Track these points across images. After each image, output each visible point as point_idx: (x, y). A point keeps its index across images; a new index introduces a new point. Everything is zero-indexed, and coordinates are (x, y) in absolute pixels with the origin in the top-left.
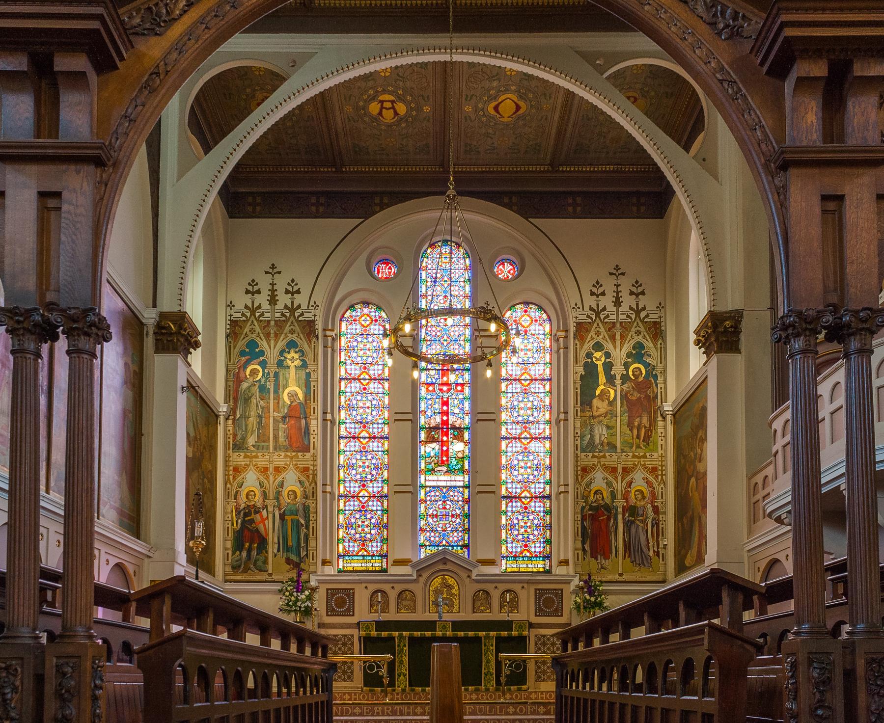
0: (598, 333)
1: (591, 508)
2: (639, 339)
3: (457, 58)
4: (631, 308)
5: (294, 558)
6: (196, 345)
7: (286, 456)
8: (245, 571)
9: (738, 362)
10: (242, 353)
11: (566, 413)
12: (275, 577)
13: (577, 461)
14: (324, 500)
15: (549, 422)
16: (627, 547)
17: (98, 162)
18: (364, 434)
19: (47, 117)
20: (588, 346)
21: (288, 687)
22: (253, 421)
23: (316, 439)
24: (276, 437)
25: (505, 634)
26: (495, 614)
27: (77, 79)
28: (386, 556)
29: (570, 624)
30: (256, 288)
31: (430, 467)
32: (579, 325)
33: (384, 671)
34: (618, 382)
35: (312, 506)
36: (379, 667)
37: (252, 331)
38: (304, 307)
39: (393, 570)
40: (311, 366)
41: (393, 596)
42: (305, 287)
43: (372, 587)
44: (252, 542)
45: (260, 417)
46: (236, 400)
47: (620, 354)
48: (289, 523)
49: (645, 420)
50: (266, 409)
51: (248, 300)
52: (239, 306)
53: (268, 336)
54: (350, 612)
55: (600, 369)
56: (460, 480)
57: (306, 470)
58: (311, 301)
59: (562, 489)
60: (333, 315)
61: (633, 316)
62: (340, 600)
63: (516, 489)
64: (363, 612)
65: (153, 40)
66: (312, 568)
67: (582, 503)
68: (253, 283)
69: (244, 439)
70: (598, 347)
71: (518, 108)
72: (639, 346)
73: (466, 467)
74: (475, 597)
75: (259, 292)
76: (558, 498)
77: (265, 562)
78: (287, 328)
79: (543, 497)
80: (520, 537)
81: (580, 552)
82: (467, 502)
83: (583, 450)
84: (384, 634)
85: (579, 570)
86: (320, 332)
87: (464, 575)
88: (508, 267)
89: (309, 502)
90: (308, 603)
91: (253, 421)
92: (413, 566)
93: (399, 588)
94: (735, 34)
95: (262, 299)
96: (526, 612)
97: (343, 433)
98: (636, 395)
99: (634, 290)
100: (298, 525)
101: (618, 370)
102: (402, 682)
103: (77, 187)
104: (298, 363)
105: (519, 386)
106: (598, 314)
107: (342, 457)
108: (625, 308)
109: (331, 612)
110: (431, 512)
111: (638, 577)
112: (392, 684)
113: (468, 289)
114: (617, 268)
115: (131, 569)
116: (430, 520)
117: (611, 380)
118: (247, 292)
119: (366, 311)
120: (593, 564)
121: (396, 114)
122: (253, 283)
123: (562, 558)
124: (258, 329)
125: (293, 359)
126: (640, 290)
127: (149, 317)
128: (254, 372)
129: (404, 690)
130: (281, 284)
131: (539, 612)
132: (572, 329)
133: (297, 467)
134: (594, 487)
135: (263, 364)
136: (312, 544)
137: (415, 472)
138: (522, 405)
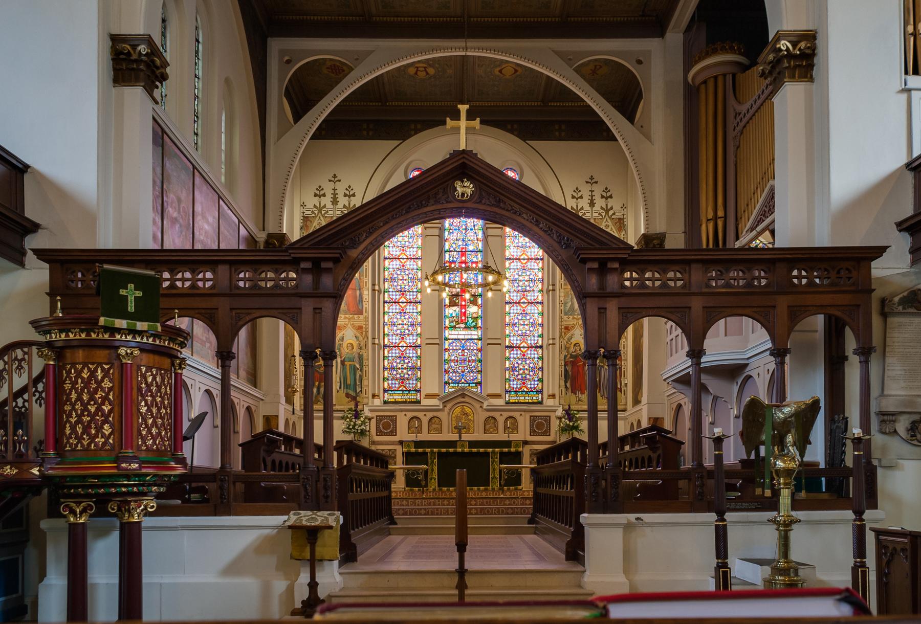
1: (572, 356)
3: (468, 54)
4: (602, 208)
5: (352, 393)
7: (345, 318)
11: (553, 285)
13: (561, 322)
14: (374, 350)
15: (541, 291)
17: (335, 297)
18: (403, 299)
19: (316, 283)
21: (360, 487)
23: (367, 305)
25: (506, 450)
26: (501, 436)
27: (328, 270)
28: (419, 391)
29: (555, 442)
30: (322, 192)
31: (452, 324)
33: (421, 477)
35: (365, 356)
36: (418, 474)
39: (425, 402)
41: (425, 421)
48: (348, 368)
51: (316, 201)
52: (310, 206)
54: (393, 433)
56: (475, 334)
57: (360, 328)
59: (551, 342)
61: (603, 214)
62: (387, 425)
63: (516, 341)
64: (403, 433)
65: (354, 250)
66: (365, 401)
67: (565, 353)
68: (320, 188)
71: (516, 71)
73: (479, 324)
74: (486, 421)
75: (324, 195)
76: (547, 349)
79: (537, 347)
80: (520, 377)
81: (564, 390)
82: (480, 350)
83: (566, 314)
84: (420, 450)
85: (562, 402)
87: (477, 405)
89: (363, 352)
90: (363, 427)
92: (439, 400)
95: (327, 201)
96: (523, 433)
97: (387, 299)
99: (604, 194)
100: (354, 369)
102: (433, 484)
103: (327, 305)
105: (519, 264)
107: (386, 317)
108: (597, 208)
109: (379, 432)
110: (453, 358)
112: (426, 485)
114: (592, 178)
115: (253, 408)
116: (453, 364)
118: (316, 195)
120: (573, 398)
121: (427, 73)
122: (320, 188)
123: (551, 393)
126: (609, 194)
127: (261, 237)
129: (434, 490)
130: (341, 189)
131: (533, 432)
133: (353, 326)
134: (574, 341)
136: (365, 382)
137: (442, 328)
138: (521, 278)
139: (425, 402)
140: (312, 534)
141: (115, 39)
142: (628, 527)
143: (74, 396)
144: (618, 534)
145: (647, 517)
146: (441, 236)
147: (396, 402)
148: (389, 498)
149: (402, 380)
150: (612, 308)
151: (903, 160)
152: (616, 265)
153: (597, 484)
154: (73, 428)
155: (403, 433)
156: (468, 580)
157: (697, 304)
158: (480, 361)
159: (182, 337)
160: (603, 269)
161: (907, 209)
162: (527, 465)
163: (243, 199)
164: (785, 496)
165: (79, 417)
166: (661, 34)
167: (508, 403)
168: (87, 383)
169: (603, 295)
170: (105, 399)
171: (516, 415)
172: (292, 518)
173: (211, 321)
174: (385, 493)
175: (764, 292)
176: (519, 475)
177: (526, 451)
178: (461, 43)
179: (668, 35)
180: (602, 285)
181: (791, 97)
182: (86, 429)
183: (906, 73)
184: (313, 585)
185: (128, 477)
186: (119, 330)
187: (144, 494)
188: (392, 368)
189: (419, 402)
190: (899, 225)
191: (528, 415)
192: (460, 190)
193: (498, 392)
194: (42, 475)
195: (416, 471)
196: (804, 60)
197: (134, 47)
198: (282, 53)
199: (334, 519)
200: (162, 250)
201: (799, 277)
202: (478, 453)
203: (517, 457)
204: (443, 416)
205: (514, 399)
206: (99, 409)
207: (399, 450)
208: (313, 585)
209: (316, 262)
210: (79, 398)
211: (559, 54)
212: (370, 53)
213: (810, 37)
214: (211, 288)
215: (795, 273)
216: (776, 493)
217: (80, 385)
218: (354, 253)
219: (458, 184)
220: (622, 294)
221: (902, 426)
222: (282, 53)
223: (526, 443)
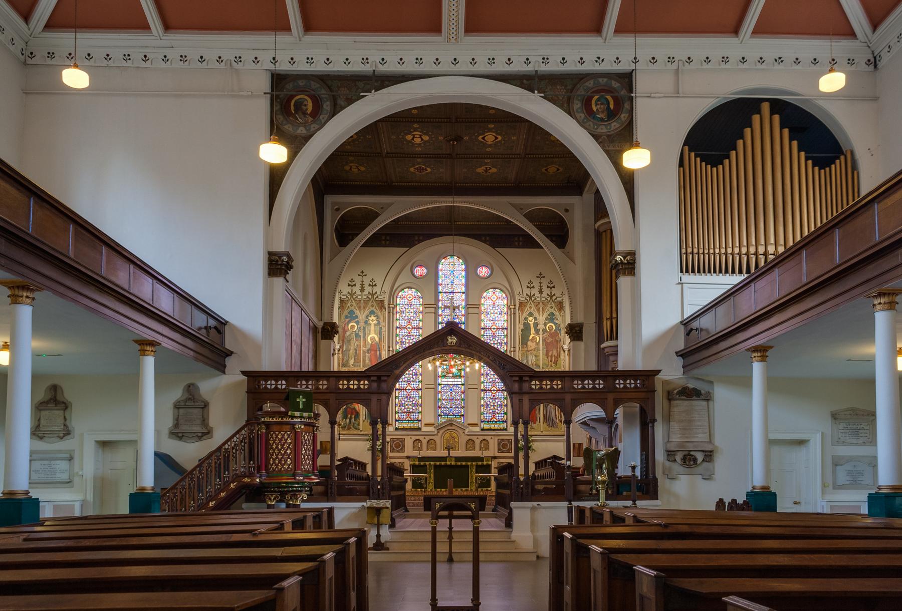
0: (531, 308)
2: (552, 310)
6: (337, 332)
8: (348, 429)
9: (581, 344)
10: (347, 317)
12: (363, 432)
16: (545, 418)
20: (525, 314)
22: (352, 352)
24: (364, 360)
26: (477, 453)
27: (385, 381)
32: (521, 303)
34: (541, 333)
37: (352, 305)
38: (378, 293)
39: (424, 429)
40: (382, 324)
41: (425, 442)
42: (379, 282)
43: (414, 438)
44: (352, 414)
45: (356, 350)
46: (343, 341)
47: (542, 318)
49: (555, 352)
50: (359, 346)
51: (349, 289)
53: (360, 308)
55: (532, 326)
56: (459, 381)
58: (382, 290)
60: (393, 295)
64: (409, 451)
69: (347, 361)
70: (531, 314)
72: (552, 314)
77: (359, 424)
78: (370, 304)
82: (463, 392)
86: (386, 306)
87: (461, 431)
88: (485, 269)
91: (352, 352)
93: (428, 438)
94: (504, 368)
95: (357, 289)
96: (493, 451)
98: (550, 339)
101: (541, 327)
103: (384, 397)
104: (375, 322)
106: (530, 297)
108: (544, 294)
111: (551, 433)
113: (464, 281)
114: (541, 274)
117: (537, 331)
119: (410, 292)
124: (354, 304)
125: (373, 320)
127: (320, 325)
128: (353, 327)
131: (500, 450)
132: (517, 306)
135: (357, 323)
139: (424, 429)
140: (378, 511)
141: (270, 254)
143: (274, 446)
144: (528, 512)
145: (543, 504)
146: (436, 313)
147: (404, 429)
148: (404, 495)
149: (409, 412)
150: (526, 399)
151: (680, 320)
152: (527, 379)
153: (518, 487)
154: (274, 461)
155: (409, 451)
156: (454, 535)
157: (568, 397)
158: (463, 400)
159: (317, 416)
160: (521, 379)
161: (681, 345)
162: (494, 473)
163: (311, 307)
164: (602, 492)
165: (277, 456)
166: (580, 194)
167: (483, 429)
168: (280, 440)
169: (521, 393)
170: (288, 447)
171: (488, 438)
172: (368, 504)
173: (326, 406)
174: (402, 492)
175: (600, 392)
176: (489, 481)
177: (494, 464)
178: (450, 199)
179: (584, 195)
180: (520, 388)
181: (624, 282)
182: (280, 461)
183: (681, 271)
184: (378, 536)
185: (298, 483)
186: (295, 417)
187: (301, 491)
188: (402, 405)
189: (420, 429)
190: (677, 353)
191: (496, 438)
192: (450, 340)
193: (476, 422)
194: (261, 482)
195: (419, 478)
196: (630, 266)
197: (280, 257)
198: (334, 204)
199: (388, 503)
200: (301, 372)
201: (619, 384)
202: (461, 466)
203: (487, 468)
204: (437, 439)
205: (486, 426)
206: (286, 452)
207: (407, 464)
208: (378, 536)
209: (379, 377)
210: (277, 447)
211: (513, 205)
212: (391, 204)
213: (633, 254)
214: (327, 388)
215: (617, 382)
216: (598, 491)
217: (277, 441)
218: (397, 372)
219: (449, 338)
220: (531, 392)
221: (679, 457)
222: (334, 204)
223: (495, 458)
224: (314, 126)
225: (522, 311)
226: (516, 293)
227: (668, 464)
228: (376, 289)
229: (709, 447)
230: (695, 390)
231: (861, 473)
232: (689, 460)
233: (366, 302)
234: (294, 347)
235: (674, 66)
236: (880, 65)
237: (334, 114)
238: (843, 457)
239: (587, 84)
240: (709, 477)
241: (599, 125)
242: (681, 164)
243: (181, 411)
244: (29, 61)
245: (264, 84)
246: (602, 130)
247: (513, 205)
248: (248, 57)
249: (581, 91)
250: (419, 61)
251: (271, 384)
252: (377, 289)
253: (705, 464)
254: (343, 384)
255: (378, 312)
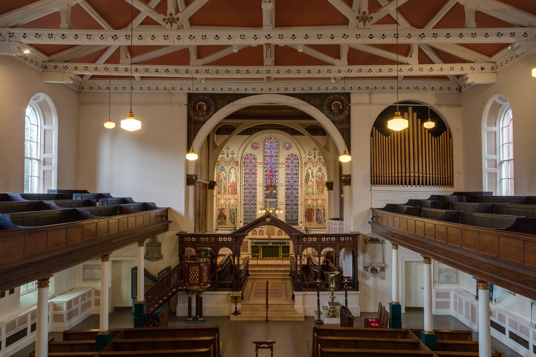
8: (221, 224)
10: (220, 169)
16: (317, 219)
20: (307, 168)
22: (223, 187)
40: (237, 173)
47: (315, 170)
49: (321, 187)
69: (220, 191)
70: (310, 168)
72: (320, 168)
86: (239, 164)
100: (234, 213)
101: (315, 174)
108: (316, 158)
117: (313, 177)
142: (304, 295)
144: (301, 297)
145: (308, 293)
157: (319, 245)
183: (371, 184)
184: (236, 308)
202: (275, 246)
208: (236, 308)
211: (300, 124)
212: (242, 123)
213: (350, 176)
221: (369, 269)
224: (207, 117)
225: (306, 166)
226: (303, 158)
227: (365, 272)
228: (234, 156)
229: (383, 265)
230: (376, 239)
231: (451, 277)
232: (374, 270)
233: (230, 162)
234: (197, 203)
235: (369, 91)
236: (462, 91)
237: (216, 111)
238: (443, 269)
239: (330, 97)
240: (383, 278)
241: (335, 116)
242: (372, 135)
243: (149, 248)
244: (82, 91)
245: (185, 99)
246: (337, 118)
247: (300, 124)
248: (178, 88)
249: (327, 101)
250: (254, 89)
251: (189, 239)
252: (235, 156)
253: (381, 272)
254: (220, 239)
255: (235, 167)
